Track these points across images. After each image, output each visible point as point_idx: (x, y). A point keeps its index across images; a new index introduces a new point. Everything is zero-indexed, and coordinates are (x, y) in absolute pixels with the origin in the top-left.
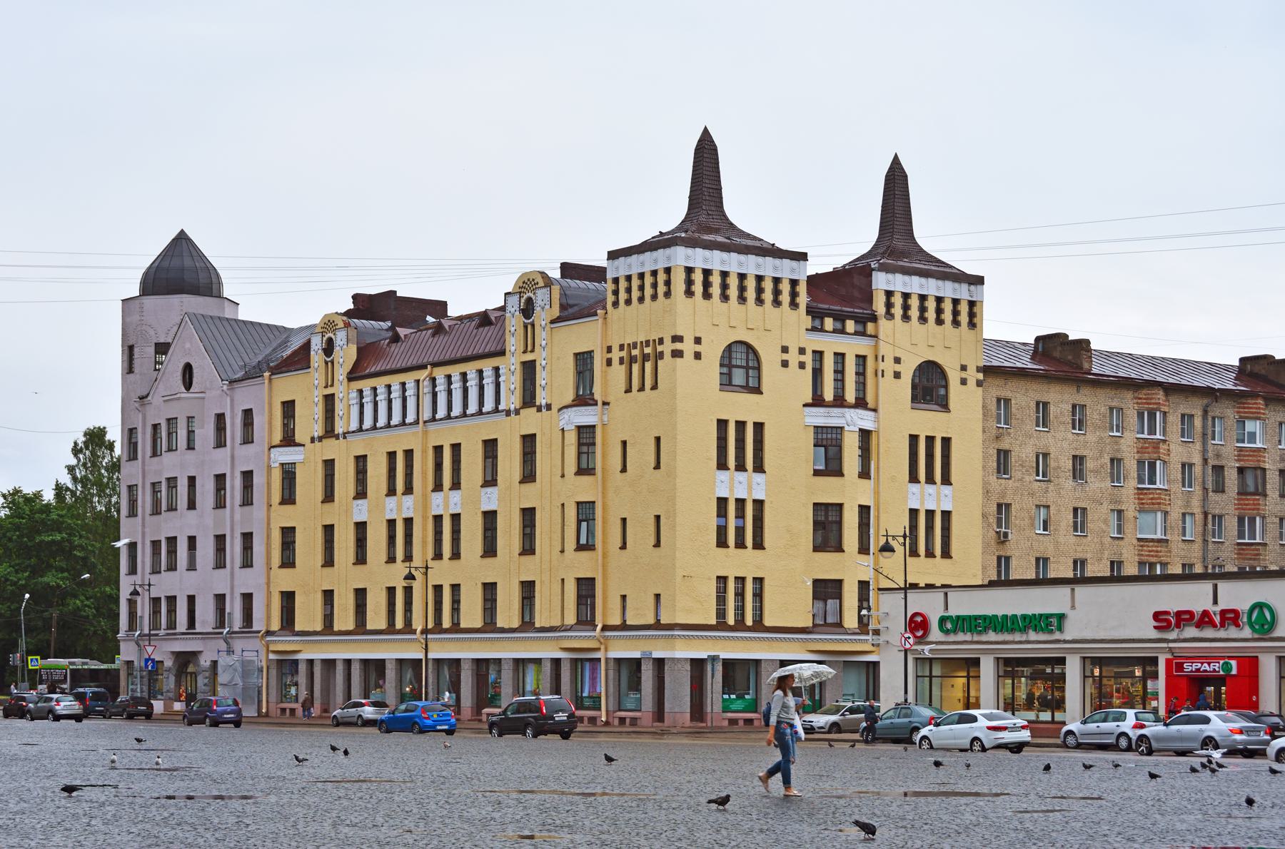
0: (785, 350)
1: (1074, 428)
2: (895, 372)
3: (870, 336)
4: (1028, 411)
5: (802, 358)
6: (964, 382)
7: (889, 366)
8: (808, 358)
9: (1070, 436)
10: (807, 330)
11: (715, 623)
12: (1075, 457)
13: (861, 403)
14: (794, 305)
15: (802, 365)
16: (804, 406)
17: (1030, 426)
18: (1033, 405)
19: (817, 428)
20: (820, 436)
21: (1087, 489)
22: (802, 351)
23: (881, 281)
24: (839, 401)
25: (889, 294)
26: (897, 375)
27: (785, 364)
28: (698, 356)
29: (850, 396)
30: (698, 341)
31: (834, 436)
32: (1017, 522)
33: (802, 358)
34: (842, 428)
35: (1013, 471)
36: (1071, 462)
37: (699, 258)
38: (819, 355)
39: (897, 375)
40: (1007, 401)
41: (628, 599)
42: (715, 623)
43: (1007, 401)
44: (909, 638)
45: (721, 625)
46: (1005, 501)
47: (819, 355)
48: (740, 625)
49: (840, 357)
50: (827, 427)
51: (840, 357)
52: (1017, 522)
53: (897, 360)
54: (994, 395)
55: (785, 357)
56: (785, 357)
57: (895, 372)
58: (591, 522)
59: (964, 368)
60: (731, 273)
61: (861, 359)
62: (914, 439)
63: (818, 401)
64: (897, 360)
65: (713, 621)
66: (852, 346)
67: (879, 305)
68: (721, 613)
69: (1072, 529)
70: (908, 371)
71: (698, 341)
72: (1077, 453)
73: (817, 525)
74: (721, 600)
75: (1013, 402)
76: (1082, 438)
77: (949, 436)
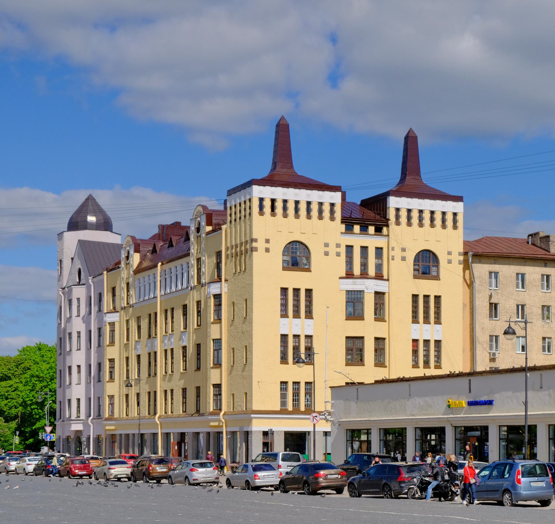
0: (327, 245)
1: (543, 288)
2: (325, 244)
3: (385, 236)
4: (510, 279)
5: (338, 250)
6: (450, 262)
7: (397, 254)
8: (343, 250)
9: (540, 294)
10: (341, 233)
11: (279, 410)
12: (543, 306)
13: (379, 276)
14: (332, 219)
15: (338, 254)
16: (340, 278)
17: (512, 288)
18: (514, 275)
19: (348, 292)
20: (350, 296)
21: (552, 326)
22: (338, 246)
23: (393, 202)
24: (364, 275)
25: (398, 210)
26: (404, 259)
27: (326, 254)
28: (267, 250)
29: (372, 271)
30: (267, 241)
31: (359, 296)
32: (504, 347)
33: (338, 250)
34: (363, 291)
35: (500, 315)
36: (541, 310)
37: (279, 193)
38: (350, 248)
39: (404, 259)
40: (496, 274)
41: (174, 391)
42: (279, 410)
43: (496, 274)
44: (316, 417)
45: (283, 411)
46: (495, 334)
47: (350, 248)
48: (296, 410)
49: (364, 249)
50: (355, 291)
51: (364, 249)
52: (504, 347)
53: (404, 250)
54: (487, 270)
55: (327, 249)
56: (327, 249)
57: (325, 244)
58: (219, 350)
59: (449, 253)
60: (301, 201)
61: (379, 250)
62: (415, 297)
63: (349, 275)
64: (404, 250)
65: (278, 408)
66: (380, 242)
67: (392, 214)
68: (284, 403)
69: (542, 350)
70: (411, 257)
71: (267, 241)
72: (545, 304)
73: (349, 350)
74: (283, 396)
75: (500, 273)
76: (548, 295)
77: (439, 295)
